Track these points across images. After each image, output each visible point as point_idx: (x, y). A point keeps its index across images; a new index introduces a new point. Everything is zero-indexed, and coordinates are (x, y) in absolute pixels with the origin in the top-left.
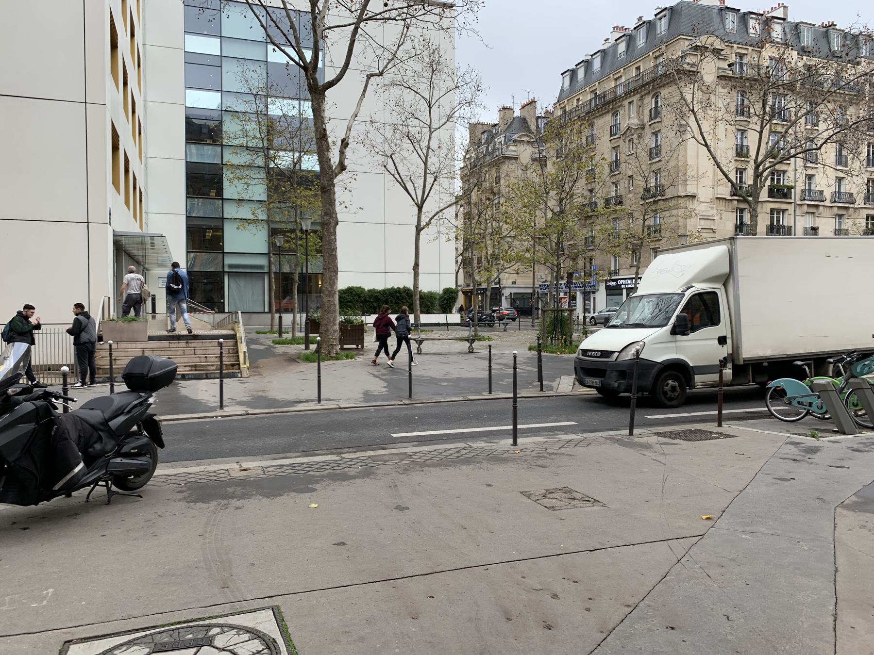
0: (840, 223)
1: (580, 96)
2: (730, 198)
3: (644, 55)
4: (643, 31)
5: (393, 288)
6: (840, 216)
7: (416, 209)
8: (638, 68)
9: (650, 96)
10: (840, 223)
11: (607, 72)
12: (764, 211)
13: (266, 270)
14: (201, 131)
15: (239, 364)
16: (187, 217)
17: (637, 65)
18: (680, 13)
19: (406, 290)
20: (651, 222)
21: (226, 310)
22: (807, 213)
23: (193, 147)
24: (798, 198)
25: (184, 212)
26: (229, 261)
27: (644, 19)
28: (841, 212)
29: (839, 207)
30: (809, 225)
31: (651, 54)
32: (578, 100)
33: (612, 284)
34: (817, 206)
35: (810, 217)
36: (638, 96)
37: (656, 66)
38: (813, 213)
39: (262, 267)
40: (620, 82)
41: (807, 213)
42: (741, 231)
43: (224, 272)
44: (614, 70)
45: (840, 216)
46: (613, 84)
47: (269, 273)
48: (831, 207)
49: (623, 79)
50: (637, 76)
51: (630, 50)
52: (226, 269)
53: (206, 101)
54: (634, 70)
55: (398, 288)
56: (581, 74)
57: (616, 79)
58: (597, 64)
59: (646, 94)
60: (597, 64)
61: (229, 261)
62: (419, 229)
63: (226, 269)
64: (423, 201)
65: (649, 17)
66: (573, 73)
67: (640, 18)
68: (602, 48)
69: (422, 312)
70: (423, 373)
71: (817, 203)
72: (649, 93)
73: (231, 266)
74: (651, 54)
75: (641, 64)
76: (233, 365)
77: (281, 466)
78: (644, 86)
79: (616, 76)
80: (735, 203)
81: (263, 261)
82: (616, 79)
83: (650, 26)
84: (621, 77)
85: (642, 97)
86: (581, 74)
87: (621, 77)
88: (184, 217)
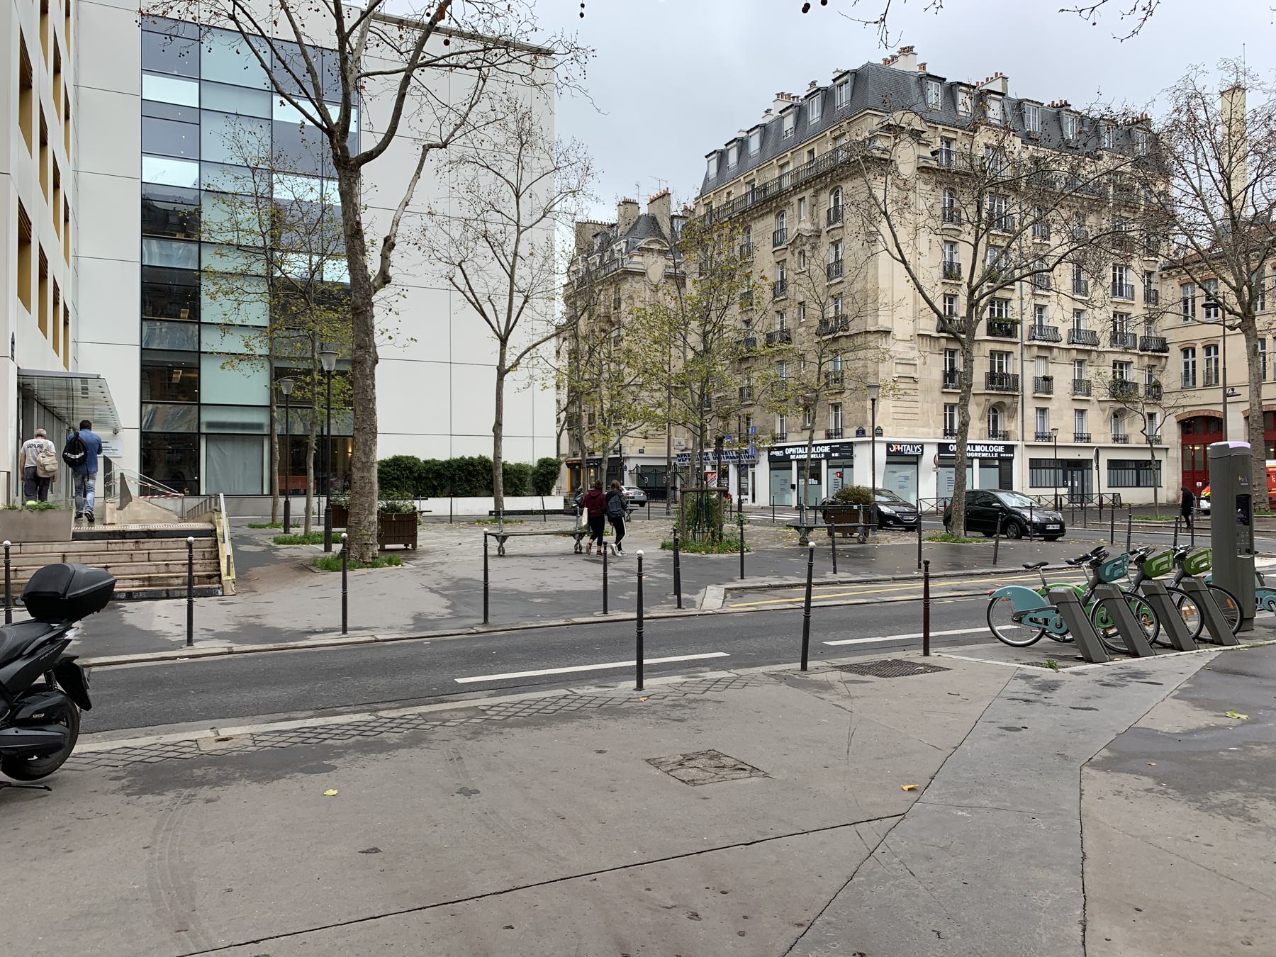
0: (1080, 371)
1: (732, 189)
3: (818, 133)
4: (817, 101)
6: (1080, 362)
8: (811, 152)
9: (828, 192)
10: (1080, 371)
11: (769, 155)
12: (982, 353)
13: (266, 431)
14: (164, 219)
16: (144, 351)
17: (810, 148)
19: (483, 461)
21: (203, 492)
25: (138, 343)
26: (207, 416)
27: (818, 85)
28: (1081, 357)
29: (1078, 350)
32: (729, 194)
34: (1050, 348)
35: (1041, 363)
36: (811, 191)
39: (260, 426)
40: (786, 170)
41: (1038, 357)
42: (952, 381)
43: (199, 434)
44: (778, 154)
45: (1080, 362)
46: (777, 173)
49: (791, 167)
50: (809, 163)
52: (204, 430)
55: (471, 458)
56: (733, 156)
57: (781, 167)
61: (207, 416)
62: (502, 373)
63: (204, 430)
64: (508, 331)
65: (825, 82)
66: (722, 155)
67: (813, 83)
68: (761, 122)
69: (506, 494)
72: (826, 187)
73: (210, 425)
75: (815, 146)
76: (210, 577)
78: (819, 177)
80: (944, 341)
81: (261, 418)
82: (781, 167)
83: (828, 95)
84: (788, 163)
85: (816, 192)
86: (733, 156)
88: (138, 349)
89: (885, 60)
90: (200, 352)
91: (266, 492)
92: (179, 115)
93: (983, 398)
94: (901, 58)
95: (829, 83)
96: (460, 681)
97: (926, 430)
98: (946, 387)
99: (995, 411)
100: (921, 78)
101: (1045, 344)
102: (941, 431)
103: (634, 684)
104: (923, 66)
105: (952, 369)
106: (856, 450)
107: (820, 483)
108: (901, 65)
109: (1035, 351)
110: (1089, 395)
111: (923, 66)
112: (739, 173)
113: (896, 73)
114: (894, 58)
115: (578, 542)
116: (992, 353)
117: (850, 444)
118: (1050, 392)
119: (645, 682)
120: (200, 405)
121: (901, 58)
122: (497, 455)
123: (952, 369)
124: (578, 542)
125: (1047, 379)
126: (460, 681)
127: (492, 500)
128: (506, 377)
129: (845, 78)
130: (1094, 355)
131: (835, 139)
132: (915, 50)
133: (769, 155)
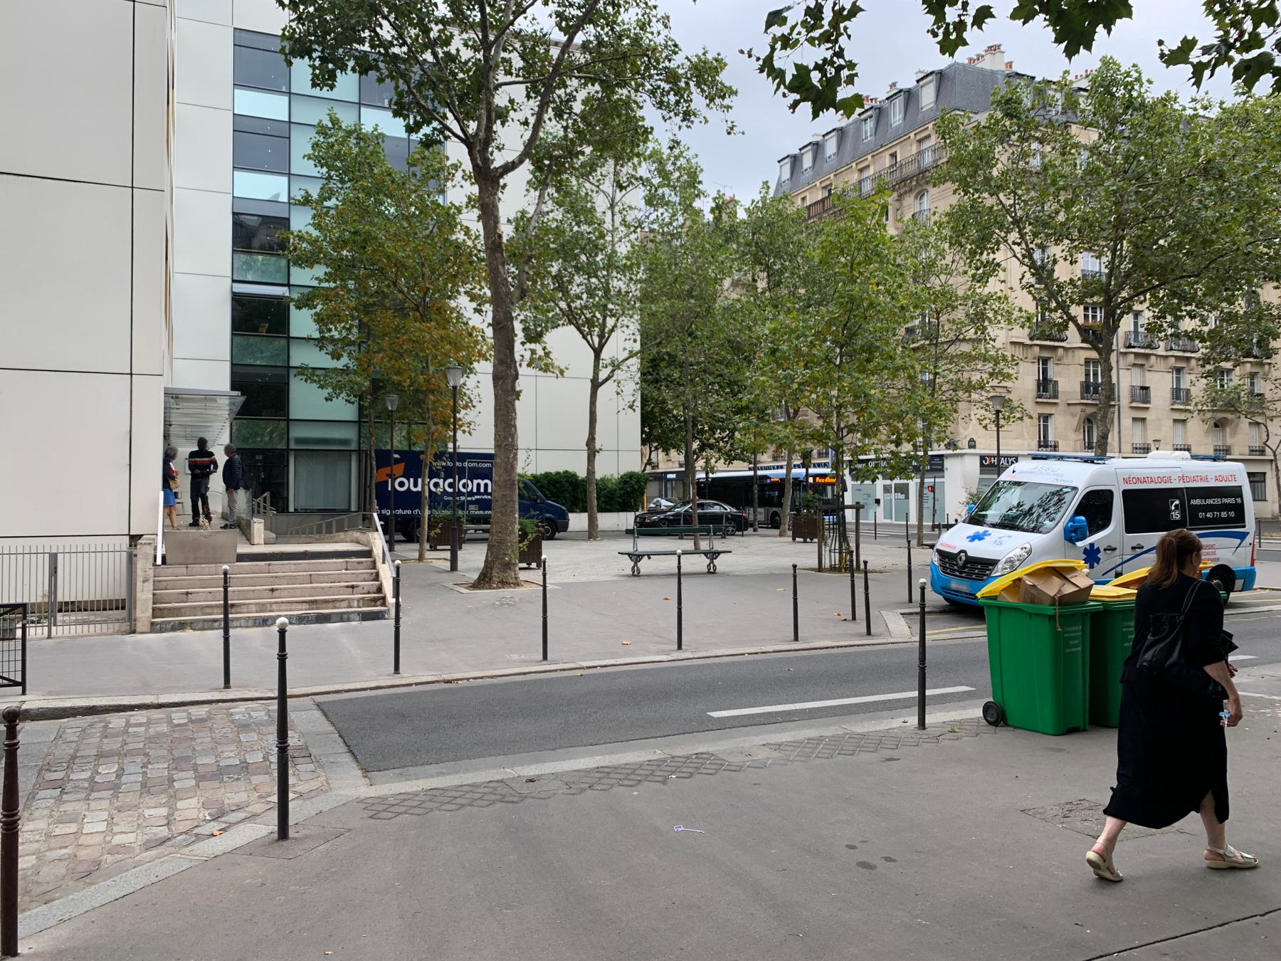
0: (1178, 380)
1: (807, 194)
2: (1029, 342)
3: (901, 137)
4: (899, 103)
5: (547, 474)
6: (1179, 370)
7: (592, 354)
8: (894, 155)
9: (913, 196)
10: (1178, 380)
11: (847, 159)
12: (1076, 361)
13: (354, 446)
14: (255, 234)
15: (384, 598)
16: (233, 365)
17: (892, 151)
18: (954, 78)
19: (569, 478)
20: (538, 348)
21: (291, 509)
22: (1134, 365)
23: (244, 257)
24: (1121, 344)
25: (228, 357)
26: (296, 432)
27: (899, 86)
28: (1179, 365)
29: (1176, 357)
30: (1138, 383)
31: (912, 135)
32: (804, 199)
33: (859, 466)
34: (1147, 356)
35: (1136, 371)
36: (895, 195)
37: (920, 153)
38: (1142, 365)
39: (345, 442)
40: (866, 174)
41: (1134, 365)
42: (1045, 390)
43: (288, 450)
44: (858, 157)
45: (1179, 370)
46: (855, 177)
47: (359, 451)
48: (1167, 357)
49: (871, 171)
50: (892, 166)
51: (880, 129)
52: (292, 446)
53: (265, 188)
54: (888, 158)
55: (558, 473)
56: (807, 161)
57: (861, 170)
58: (831, 147)
59: (906, 192)
60: (831, 147)
61: (296, 432)
62: (596, 384)
63: (292, 446)
64: (602, 346)
65: (908, 83)
66: (795, 160)
67: (894, 85)
68: (838, 125)
69: (601, 510)
70: (40, 593)
71: (1189, 355)
72: (911, 191)
73: (298, 441)
74: (912, 135)
75: (897, 149)
76: (375, 600)
77: (779, 746)
78: (904, 180)
79: (860, 166)
80: (1037, 349)
81: (350, 434)
82: (861, 170)
83: (910, 96)
84: (868, 166)
85: (900, 196)
86: (807, 161)
87: (868, 166)
88: (228, 365)
89: (970, 60)
90: (289, 367)
91: (353, 508)
92: (269, 129)
93: (1079, 408)
94: (988, 57)
95: (911, 84)
96: (715, 714)
97: (1020, 441)
98: (1040, 396)
99: (1089, 421)
100: (1009, 76)
101: (1180, 354)
102: (1035, 443)
103: (914, 720)
104: (1010, 65)
105: (1045, 378)
106: (947, 463)
107: (907, 497)
108: (987, 64)
109: (1131, 358)
110: (1056, 397)
111: (1010, 65)
112: (814, 178)
113: (982, 72)
114: (979, 57)
115: (712, 562)
116: (1087, 362)
117: (941, 457)
118: (1149, 402)
119: (929, 719)
120: (288, 420)
121: (988, 57)
122: (591, 471)
123: (1045, 378)
124: (712, 562)
125: (1145, 388)
126: (715, 714)
127: (585, 515)
128: (600, 390)
129: (930, 78)
130: (1060, 351)
131: (920, 141)
132: (1002, 48)
133: (847, 159)
